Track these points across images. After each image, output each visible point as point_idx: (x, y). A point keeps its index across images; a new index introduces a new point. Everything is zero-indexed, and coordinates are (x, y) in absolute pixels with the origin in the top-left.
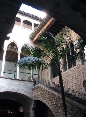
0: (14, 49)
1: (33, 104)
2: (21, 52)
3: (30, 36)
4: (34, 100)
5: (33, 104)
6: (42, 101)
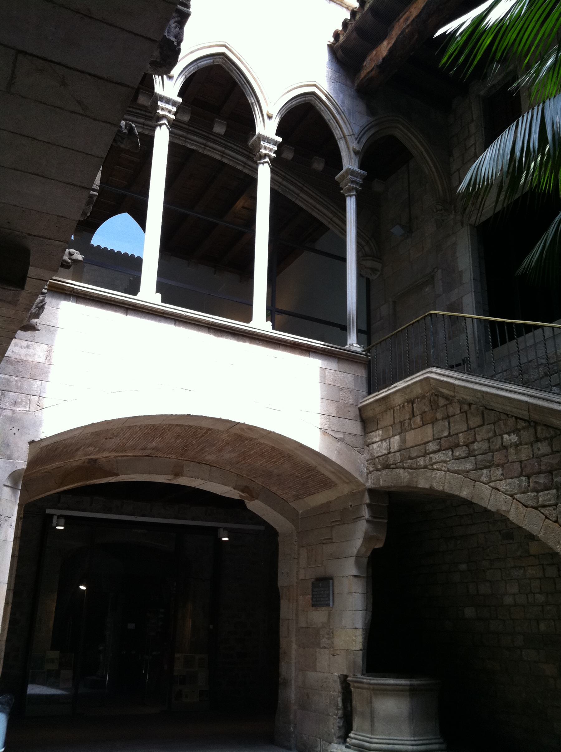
0: (214, 142)
1: (368, 501)
2: (280, 139)
3: (342, 38)
4: (372, 492)
5: (368, 501)
6: (464, 494)
